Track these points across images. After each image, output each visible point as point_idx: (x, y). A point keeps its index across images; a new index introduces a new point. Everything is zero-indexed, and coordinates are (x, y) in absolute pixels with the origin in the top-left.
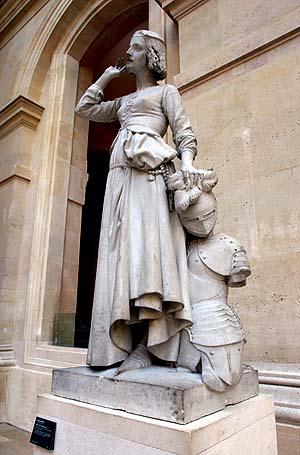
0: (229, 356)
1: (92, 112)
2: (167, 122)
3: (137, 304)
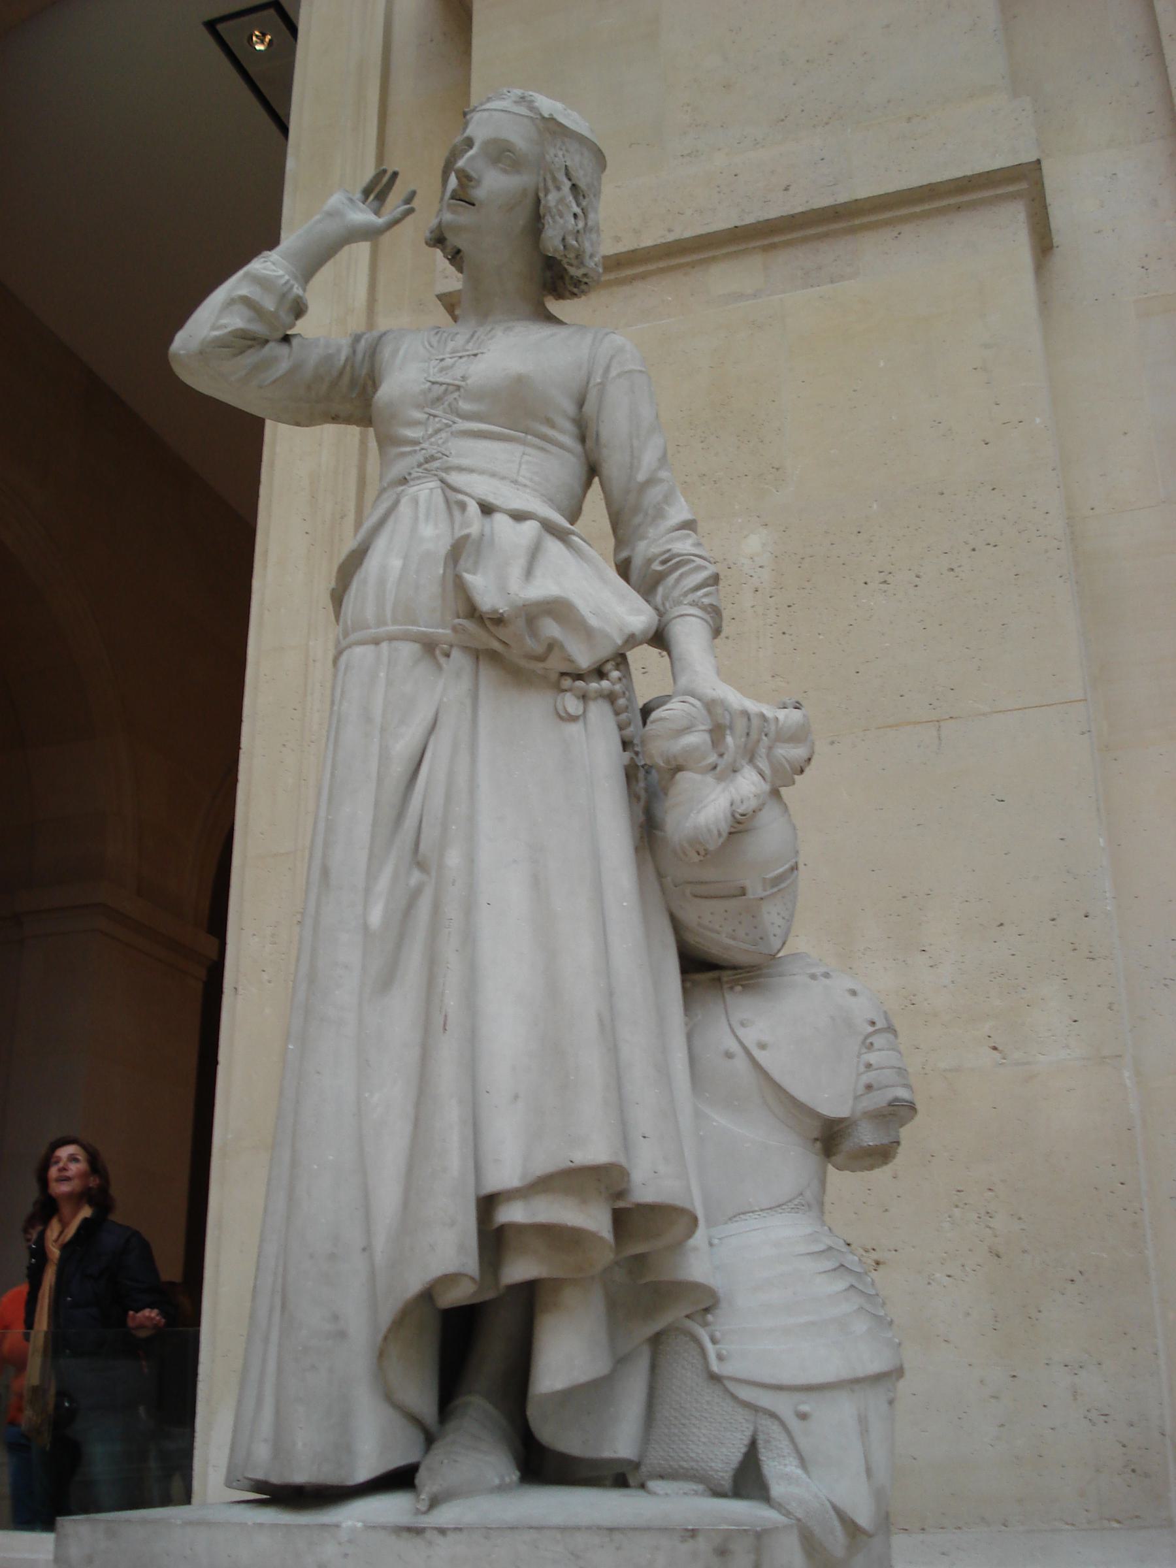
0: (863, 1421)
1: (257, 368)
2: (592, 470)
3: (512, 1214)
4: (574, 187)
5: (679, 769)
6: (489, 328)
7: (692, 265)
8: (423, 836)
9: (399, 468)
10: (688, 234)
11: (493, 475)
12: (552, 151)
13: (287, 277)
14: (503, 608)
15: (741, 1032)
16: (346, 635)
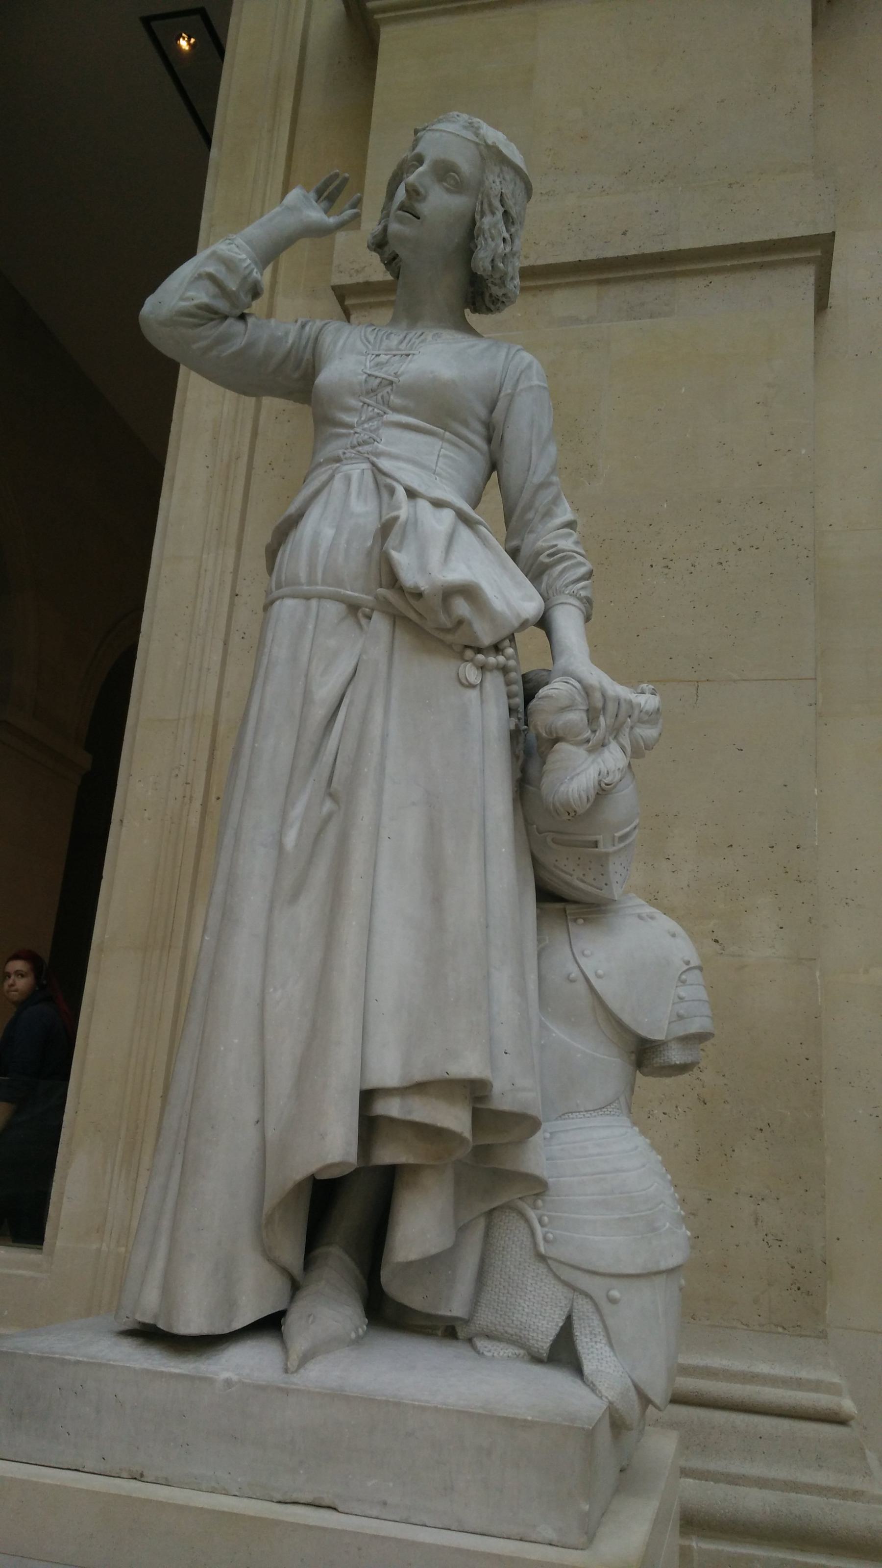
2: (494, 466)
3: (391, 1108)
4: (506, 213)
5: (557, 740)
6: (419, 333)
7: (540, 289)
9: (334, 448)
10: (541, 262)
12: (491, 178)
13: (249, 261)
14: (423, 585)
15: (582, 961)
16: (279, 586)
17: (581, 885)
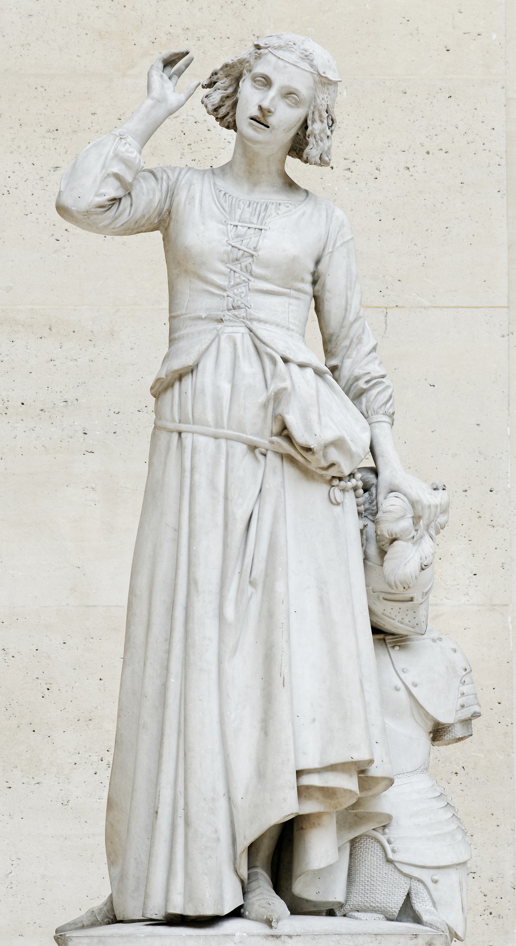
8: (254, 567)
11: (277, 325)
12: (321, 96)
15: (403, 676)
17: (399, 625)
